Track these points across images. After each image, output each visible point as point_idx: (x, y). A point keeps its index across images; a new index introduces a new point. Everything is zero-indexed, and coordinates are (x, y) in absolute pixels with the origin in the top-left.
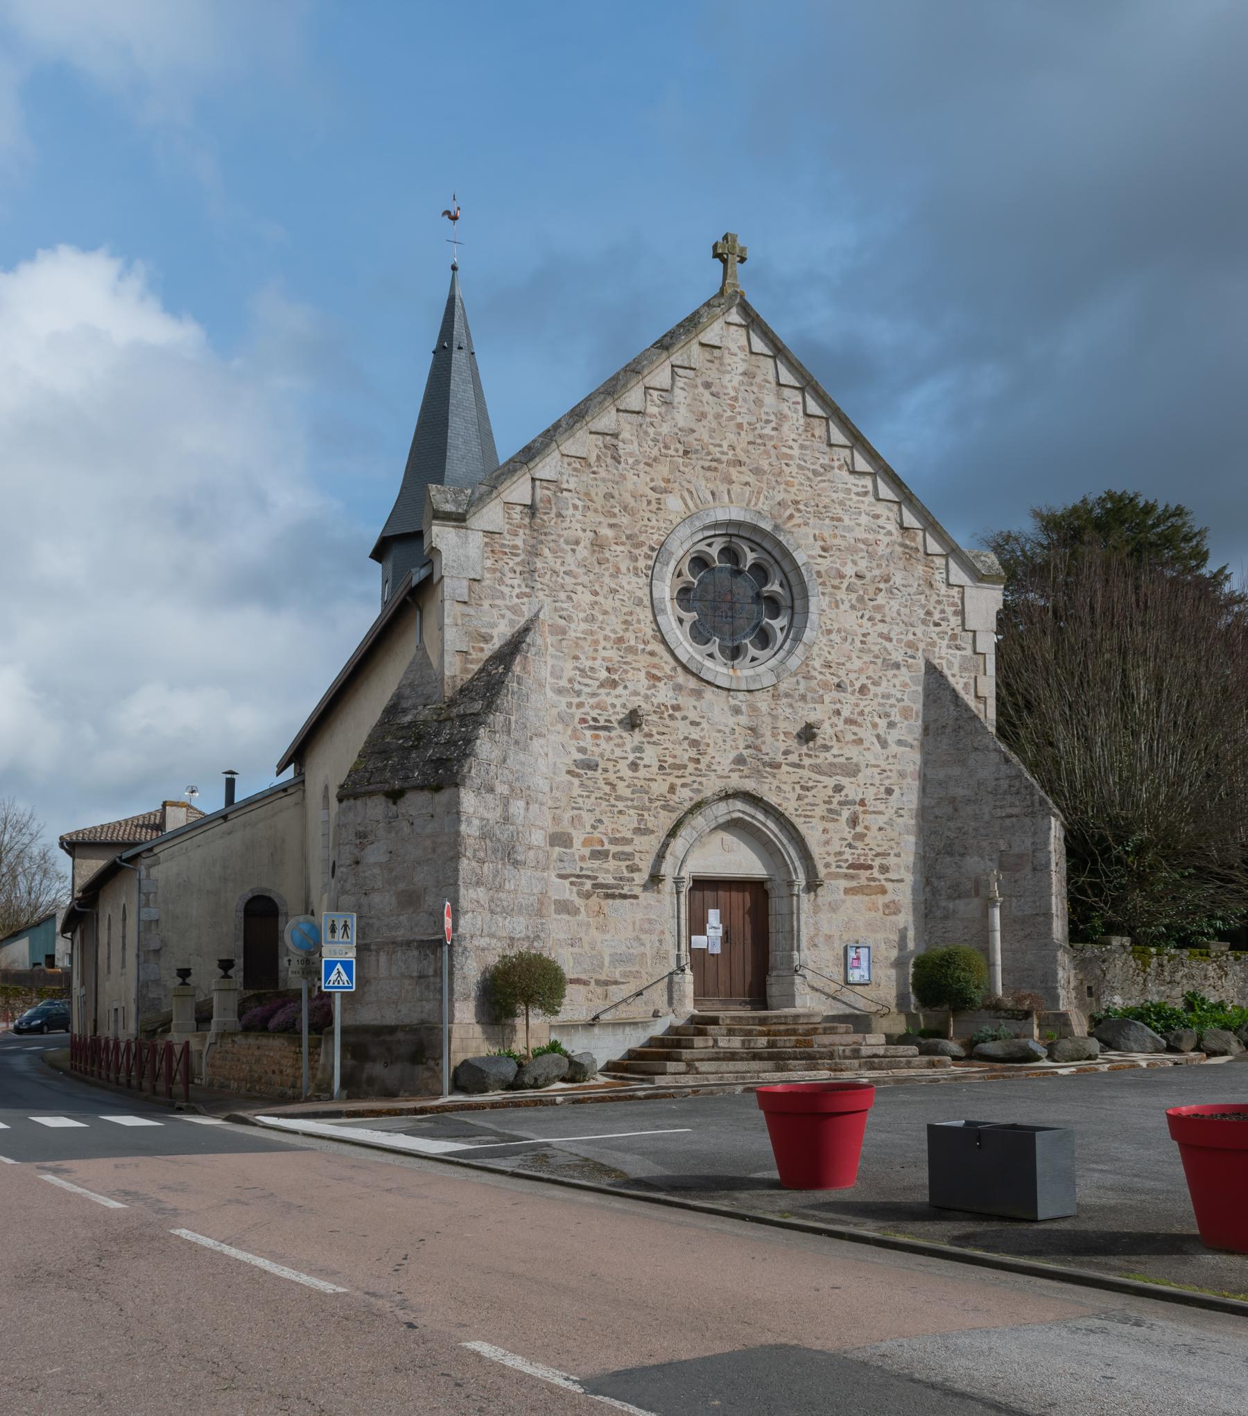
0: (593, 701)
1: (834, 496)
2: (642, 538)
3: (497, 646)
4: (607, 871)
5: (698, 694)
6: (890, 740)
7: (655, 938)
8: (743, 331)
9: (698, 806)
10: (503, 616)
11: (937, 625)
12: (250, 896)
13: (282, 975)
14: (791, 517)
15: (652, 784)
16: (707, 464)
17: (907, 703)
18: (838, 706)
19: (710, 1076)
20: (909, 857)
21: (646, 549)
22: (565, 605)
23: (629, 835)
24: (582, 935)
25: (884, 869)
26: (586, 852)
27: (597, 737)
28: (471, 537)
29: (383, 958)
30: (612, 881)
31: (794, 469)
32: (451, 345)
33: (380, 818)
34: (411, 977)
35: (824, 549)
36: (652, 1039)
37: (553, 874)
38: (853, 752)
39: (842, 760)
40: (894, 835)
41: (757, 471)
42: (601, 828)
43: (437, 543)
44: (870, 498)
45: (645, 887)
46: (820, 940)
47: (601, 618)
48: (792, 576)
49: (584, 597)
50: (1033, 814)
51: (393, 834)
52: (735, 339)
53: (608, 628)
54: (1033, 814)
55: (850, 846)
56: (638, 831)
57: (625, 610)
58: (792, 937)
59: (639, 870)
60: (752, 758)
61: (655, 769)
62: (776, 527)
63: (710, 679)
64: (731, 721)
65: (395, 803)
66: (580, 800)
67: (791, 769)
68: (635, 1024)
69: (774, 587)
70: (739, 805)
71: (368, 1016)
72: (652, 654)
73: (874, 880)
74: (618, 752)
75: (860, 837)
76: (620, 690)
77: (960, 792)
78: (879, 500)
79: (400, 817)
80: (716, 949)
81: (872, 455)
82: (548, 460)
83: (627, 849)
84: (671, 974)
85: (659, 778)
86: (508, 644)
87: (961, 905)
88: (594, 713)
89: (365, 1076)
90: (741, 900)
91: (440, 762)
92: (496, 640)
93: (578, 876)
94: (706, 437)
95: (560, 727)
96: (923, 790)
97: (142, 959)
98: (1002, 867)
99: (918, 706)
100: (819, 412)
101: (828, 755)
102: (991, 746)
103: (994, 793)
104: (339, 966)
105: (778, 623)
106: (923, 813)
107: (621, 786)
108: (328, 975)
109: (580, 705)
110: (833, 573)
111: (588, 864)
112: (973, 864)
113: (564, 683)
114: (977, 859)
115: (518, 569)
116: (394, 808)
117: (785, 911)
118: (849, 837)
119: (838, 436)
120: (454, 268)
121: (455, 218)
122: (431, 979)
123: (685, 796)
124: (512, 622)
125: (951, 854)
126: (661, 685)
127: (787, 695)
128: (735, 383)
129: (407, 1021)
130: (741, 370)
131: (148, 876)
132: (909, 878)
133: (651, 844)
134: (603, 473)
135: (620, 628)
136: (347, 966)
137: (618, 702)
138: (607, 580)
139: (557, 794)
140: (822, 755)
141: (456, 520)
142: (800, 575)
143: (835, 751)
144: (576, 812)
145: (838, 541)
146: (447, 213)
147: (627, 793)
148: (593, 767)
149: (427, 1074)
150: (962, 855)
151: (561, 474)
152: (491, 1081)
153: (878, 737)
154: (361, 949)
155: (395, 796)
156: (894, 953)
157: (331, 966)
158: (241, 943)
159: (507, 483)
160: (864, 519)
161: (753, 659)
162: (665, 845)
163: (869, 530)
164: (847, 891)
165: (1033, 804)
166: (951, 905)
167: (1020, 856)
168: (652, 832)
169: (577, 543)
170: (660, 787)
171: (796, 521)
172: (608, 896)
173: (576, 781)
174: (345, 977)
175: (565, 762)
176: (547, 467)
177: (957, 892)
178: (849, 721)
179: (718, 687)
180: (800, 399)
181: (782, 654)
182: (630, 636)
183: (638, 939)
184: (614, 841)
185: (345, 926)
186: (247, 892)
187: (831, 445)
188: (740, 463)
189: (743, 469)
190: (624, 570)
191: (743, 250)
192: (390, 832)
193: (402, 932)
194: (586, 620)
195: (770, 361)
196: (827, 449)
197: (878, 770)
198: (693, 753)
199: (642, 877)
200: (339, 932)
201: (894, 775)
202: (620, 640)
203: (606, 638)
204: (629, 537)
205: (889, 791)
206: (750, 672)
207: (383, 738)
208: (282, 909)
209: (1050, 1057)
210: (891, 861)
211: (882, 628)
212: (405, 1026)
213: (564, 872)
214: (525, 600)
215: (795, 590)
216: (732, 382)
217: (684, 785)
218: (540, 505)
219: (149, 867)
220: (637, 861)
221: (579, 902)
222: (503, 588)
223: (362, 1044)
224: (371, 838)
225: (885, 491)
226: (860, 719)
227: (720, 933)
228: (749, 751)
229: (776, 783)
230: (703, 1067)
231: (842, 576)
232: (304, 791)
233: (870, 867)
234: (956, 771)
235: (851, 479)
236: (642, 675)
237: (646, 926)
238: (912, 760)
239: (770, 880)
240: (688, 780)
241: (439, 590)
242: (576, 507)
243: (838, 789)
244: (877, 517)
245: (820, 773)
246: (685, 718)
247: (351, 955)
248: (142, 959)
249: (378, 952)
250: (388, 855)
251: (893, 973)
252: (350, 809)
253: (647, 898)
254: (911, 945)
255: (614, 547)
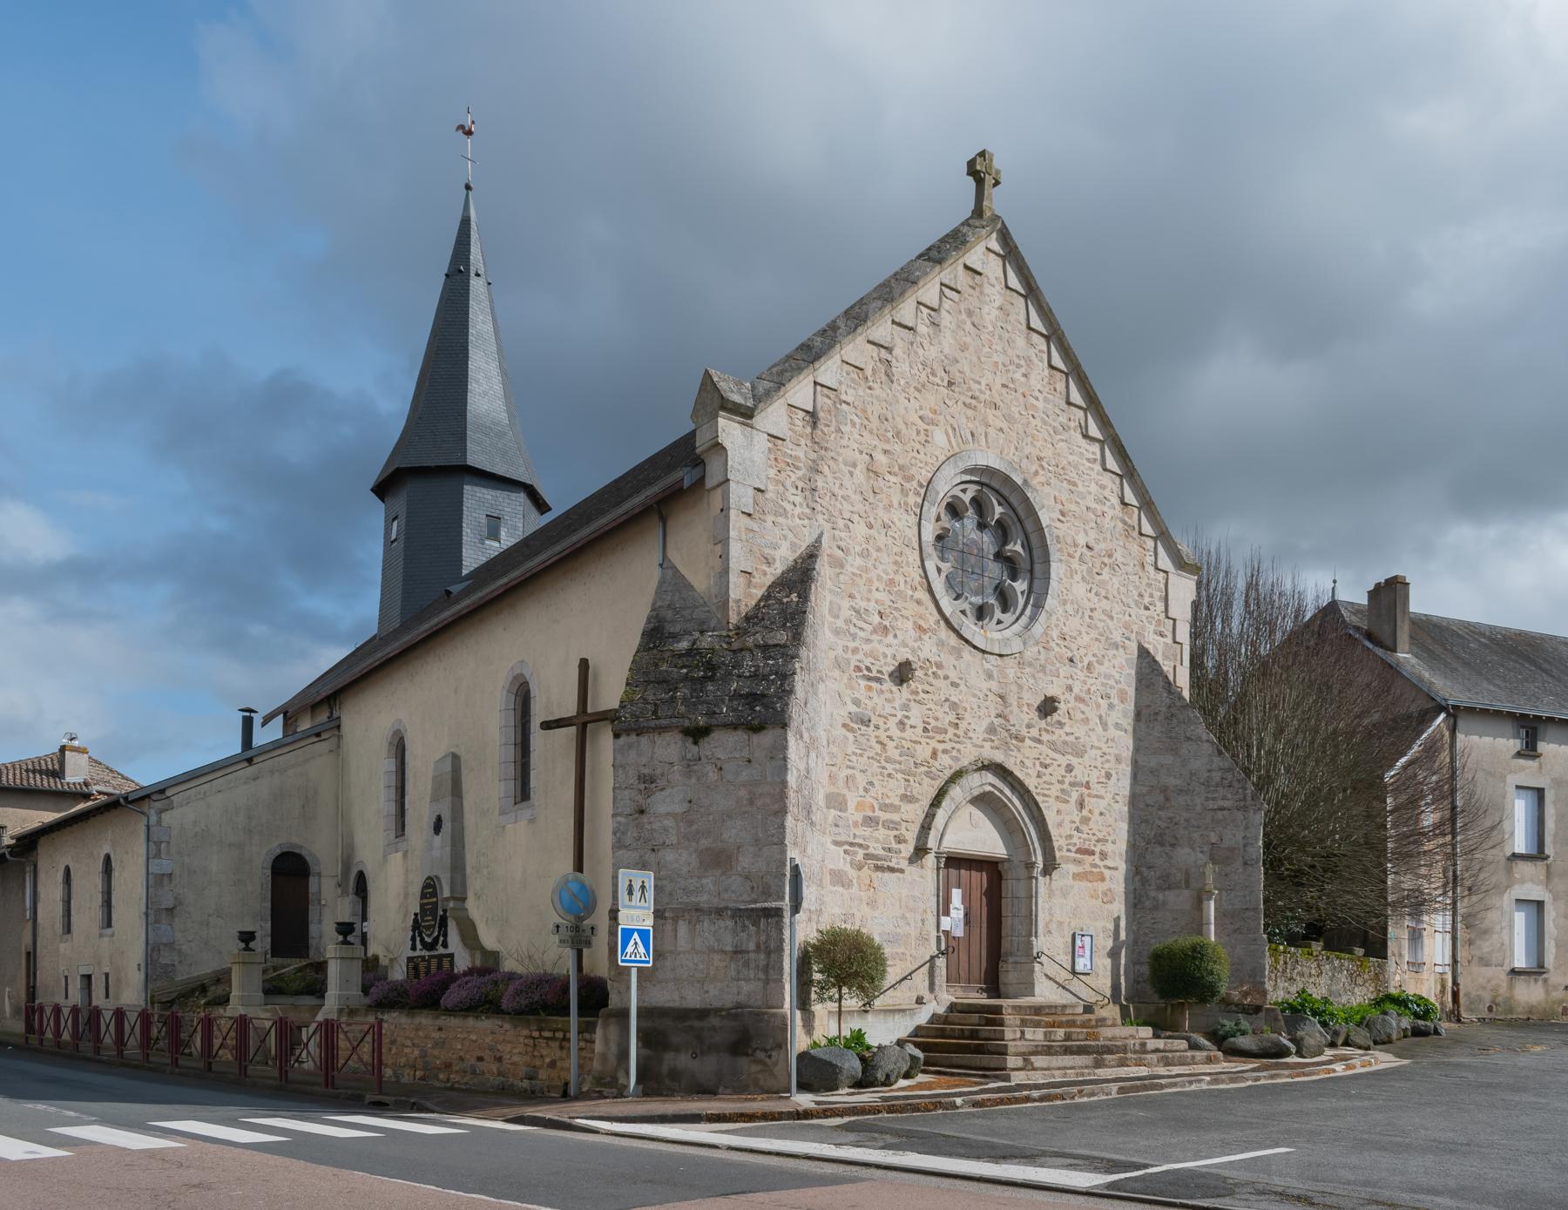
0: (867, 647)
1: (1071, 458)
2: (913, 471)
3: (779, 571)
4: (877, 841)
5: (957, 653)
6: (1111, 722)
7: (919, 917)
8: (999, 261)
9: (957, 776)
10: (785, 537)
11: (1147, 608)
12: (279, 851)
13: (313, 942)
14: (1036, 473)
15: (918, 747)
16: (969, 401)
17: (1123, 686)
18: (1070, 682)
19: (1056, 1073)
20: (1122, 846)
21: (915, 483)
22: (843, 535)
23: (897, 802)
24: (854, 911)
25: (1104, 856)
26: (859, 817)
27: (870, 688)
28: (756, 439)
29: (683, 928)
30: (882, 852)
31: (1038, 422)
32: (468, 270)
33: (675, 759)
34: (725, 952)
35: (1063, 514)
36: (918, 1028)
37: (829, 840)
38: (1080, 731)
39: (1071, 738)
40: (1111, 821)
41: (1009, 418)
42: (873, 792)
43: (723, 439)
44: (1098, 467)
45: (911, 861)
46: (1053, 927)
47: (875, 554)
48: (1034, 538)
49: (860, 529)
50: (1245, 809)
51: (694, 780)
52: (993, 267)
53: (881, 568)
54: (1245, 809)
55: (1077, 829)
56: (904, 798)
57: (896, 549)
58: (1030, 919)
59: (905, 841)
60: (1002, 729)
61: (919, 730)
62: (1025, 481)
63: (969, 637)
64: (985, 685)
65: (696, 743)
66: (854, 758)
67: (1033, 744)
68: (903, 1011)
69: (1016, 547)
70: (990, 777)
71: (665, 997)
72: (919, 602)
73: (1095, 866)
74: (888, 710)
75: (1085, 820)
76: (890, 638)
77: (1172, 782)
78: (1105, 470)
79: (704, 760)
80: (959, 932)
81: (1104, 422)
82: (829, 363)
83: (896, 817)
84: (932, 958)
85: (924, 741)
86: (793, 569)
87: (1171, 896)
88: (868, 662)
89: (665, 1068)
90: (979, 879)
91: (753, 698)
92: (778, 564)
93: (852, 844)
94: (967, 369)
95: (836, 673)
96: (1135, 777)
97: (152, 918)
98: (1213, 860)
99: (1131, 692)
100: (1062, 366)
101: (1061, 732)
102: (1204, 737)
103: (1207, 784)
104: (636, 935)
105: (1020, 586)
106: (1134, 800)
107: (890, 745)
108: (624, 949)
109: (855, 651)
110: (1069, 540)
111: (860, 831)
112: (1185, 856)
113: (840, 623)
114: (1187, 850)
115: (801, 484)
116: (695, 749)
117: (1022, 894)
118: (1077, 819)
119: (1076, 397)
120: (468, 187)
121: (469, 133)
122: (752, 956)
123: (946, 765)
124: (793, 546)
125: (1162, 844)
126: (926, 637)
127: (1031, 665)
128: (992, 317)
129: (717, 1004)
130: (997, 304)
131: (159, 822)
132: (1123, 867)
133: (916, 812)
134: (877, 391)
135: (891, 568)
136: (643, 934)
137: (889, 652)
138: (880, 512)
139: (834, 749)
140: (1058, 732)
141: (742, 415)
142: (1043, 537)
143: (1067, 729)
144: (850, 772)
145: (1073, 507)
146: (461, 127)
147: (895, 754)
148: (866, 722)
149: (755, 1068)
150: (1173, 845)
151: (841, 383)
152: (842, 1078)
153: (1100, 717)
154: (659, 914)
155: (697, 734)
156: (1110, 943)
157: (628, 934)
158: (269, 905)
159: (794, 381)
160: (1093, 488)
161: (999, 622)
162: (930, 817)
163: (1097, 501)
164: (1075, 876)
165: (1245, 799)
166: (1161, 896)
167: (1231, 850)
168: (917, 800)
169: (854, 465)
170: (923, 752)
171: (1040, 479)
172: (878, 868)
173: (850, 736)
174: (642, 949)
175: (841, 714)
176: (829, 370)
177: (1167, 884)
178: (1079, 699)
179: (975, 647)
180: (1045, 348)
181: (1024, 620)
182: (899, 578)
183: (903, 917)
184: (885, 807)
185: (643, 887)
186: (274, 847)
187: (1069, 403)
188: (996, 407)
189: (997, 413)
190: (896, 504)
191: (998, 172)
192: (689, 777)
193: (705, 897)
194: (861, 555)
195: (1022, 300)
196: (1065, 407)
197: (1099, 753)
198: (952, 717)
199: (908, 849)
200: (637, 894)
201: (1112, 758)
202: (892, 582)
203: (879, 578)
204: (901, 468)
205: (1108, 776)
206: (997, 635)
207: (656, 665)
208: (314, 868)
209: (1299, 1054)
210: (1109, 848)
211: (1105, 604)
212: (720, 1010)
213: (839, 839)
214: (806, 522)
215: (1035, 553)
216: (990, 314)
217: (945, 751)
218: (821, 415)
219: (161, 811)
220: (903, 831)
221: (852, 873)
222: (785, 504)
223: (662, 1029)
224: (661, 783)
225: (1112, 463)
226: (1087, 697)
227: (961, 914)
228: (1000, 720)
229: (1020, 758)
230: (1039, 1061)
231: (1076, 545)
232: (339, 737)
233: (1093, 853)
234: (1168, 760)
235: (1083, 443)
236: (910, 625)
237: (911, 903)
238: (1125, 744)
239: (1008, 860)
240: (948, 746)
241: (716, 499)
242: (853, 424)
243: (1070, 768)
244: (1103, 487)
245: (1055, 750)
246: (946, 678)
247: (648, 924)
248: (152, 918)
249: (675, 920)
250: (686, 805)
251: (1108, 962)
252: (630, 746)
253: (912, 871)
254: (1123, 936)
255: (888, 477)
